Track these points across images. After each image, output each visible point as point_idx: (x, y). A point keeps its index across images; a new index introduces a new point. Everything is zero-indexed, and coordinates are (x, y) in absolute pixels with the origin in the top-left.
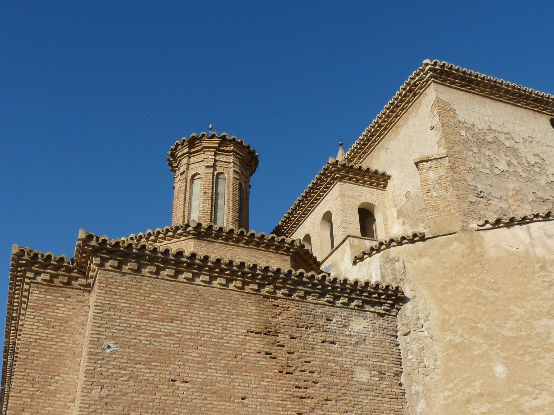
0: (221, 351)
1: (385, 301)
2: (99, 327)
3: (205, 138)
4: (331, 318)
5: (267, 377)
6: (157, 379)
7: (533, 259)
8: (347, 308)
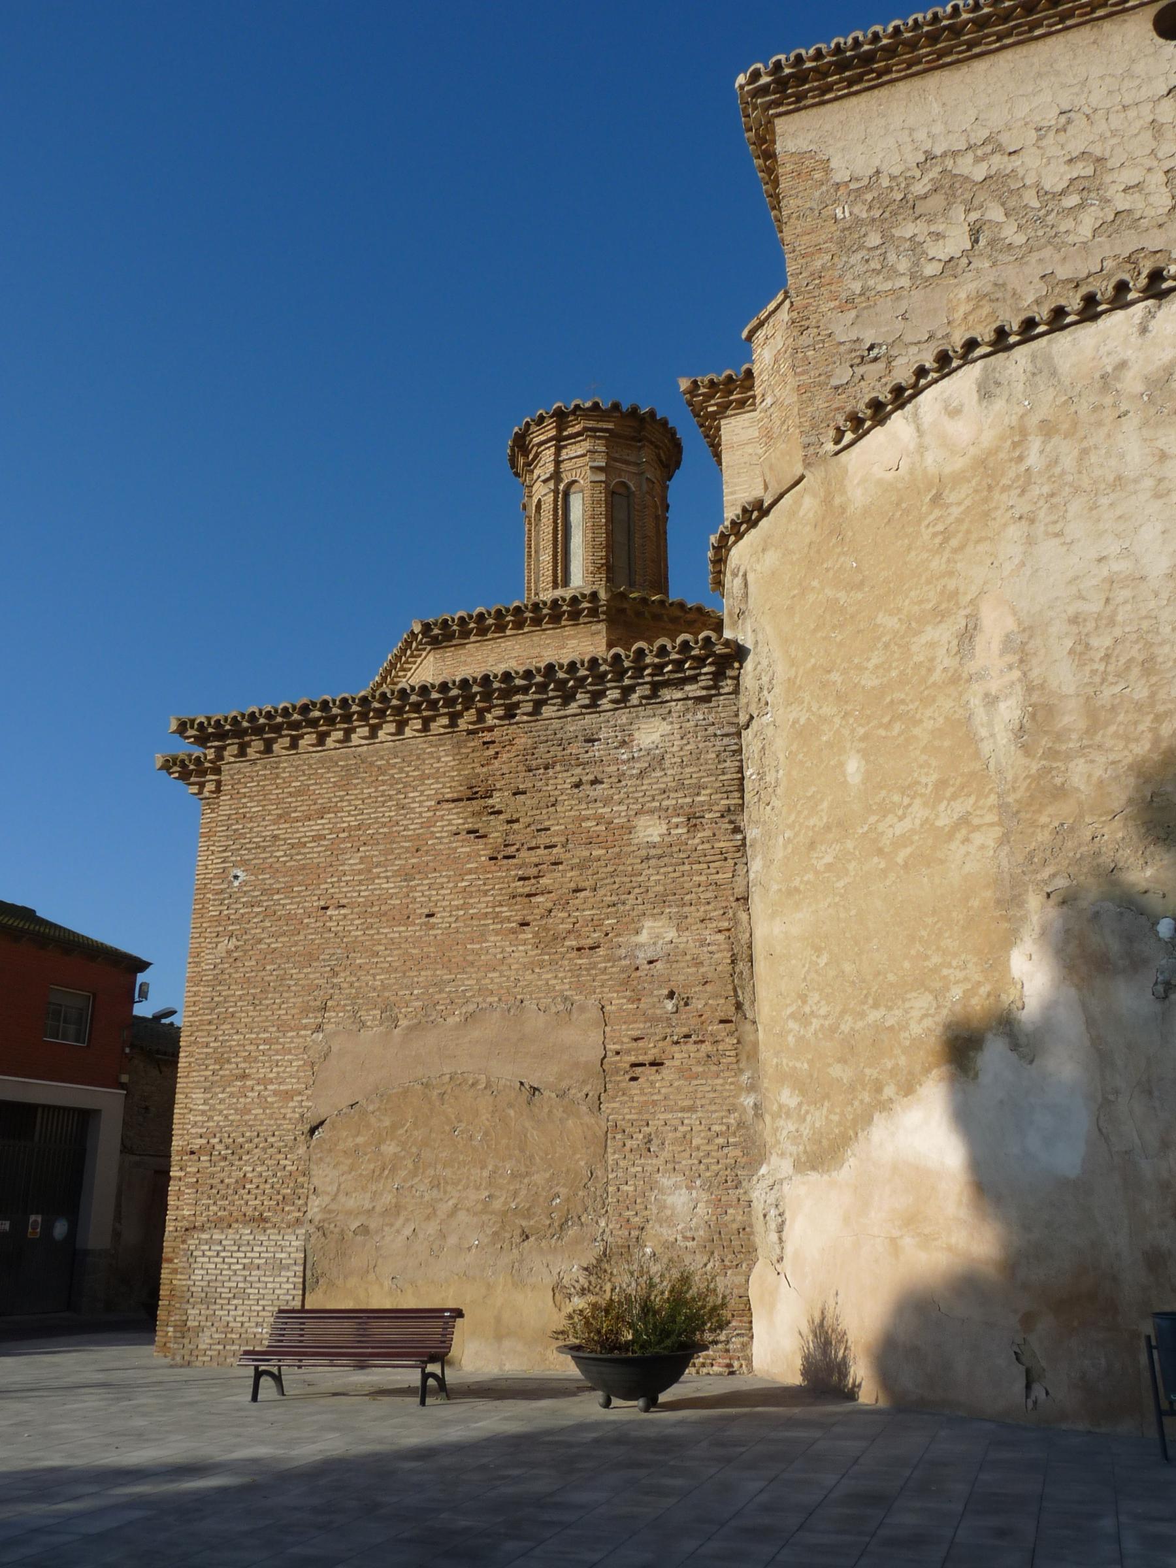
0: (394, 846)
1: (698, 671)
2: (224, 851)
3: (533, 428)
4: (596, 737)
5: (470, 872)
6: (301, 911)
7: (922, 486)
8: (626, 707)
